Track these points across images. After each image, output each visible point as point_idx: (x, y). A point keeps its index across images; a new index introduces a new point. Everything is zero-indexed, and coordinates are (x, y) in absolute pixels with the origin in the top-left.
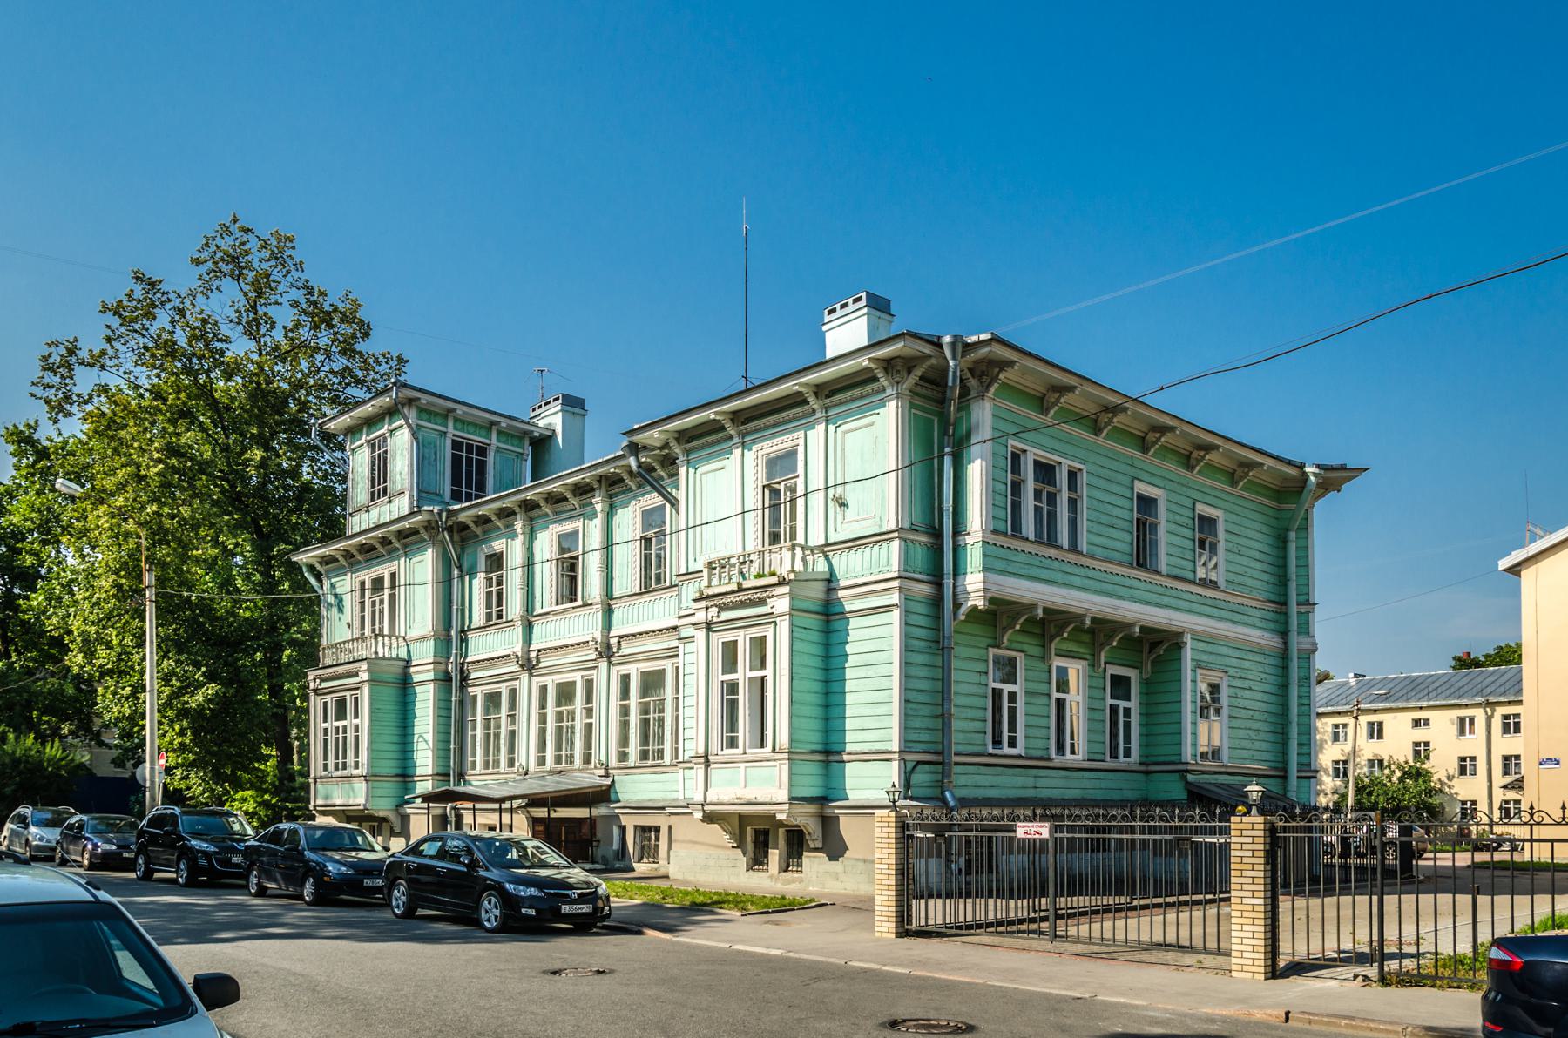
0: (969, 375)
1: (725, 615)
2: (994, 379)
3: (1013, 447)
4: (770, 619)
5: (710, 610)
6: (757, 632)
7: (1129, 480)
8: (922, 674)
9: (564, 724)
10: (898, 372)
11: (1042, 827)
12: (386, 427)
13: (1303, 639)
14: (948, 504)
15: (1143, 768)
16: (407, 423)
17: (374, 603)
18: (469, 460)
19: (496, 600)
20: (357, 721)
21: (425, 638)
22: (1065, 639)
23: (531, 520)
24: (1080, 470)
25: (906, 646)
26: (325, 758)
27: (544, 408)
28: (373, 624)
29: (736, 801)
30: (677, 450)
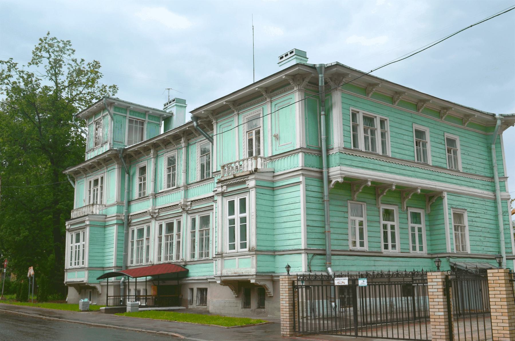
0: (330, 80)
1: (230, 189)
2: (341, 81)
3: (352, 110)
4: (247, 190)
5: (223, 187)
6: (242, 196)
7: (411, 123)
8: (315, 213)
9: (169, 242)
10: (299, 80)
11: (345, 279)
12: (101, 115)
13: (504, 194)
14: (323, 137)
15: (430, 256)
16: (109, 112)
17: (94, 190)
19: (142, 186)
20: (84, 243)
21: (113, 205)
22: (410, 199)
23: (157, 151)
24: (386, 120)
25: (306, 200)
26: (71, 260)
27: (169, 104)
28: (94, 199)
29: (234, 275)
30: (211, 117)
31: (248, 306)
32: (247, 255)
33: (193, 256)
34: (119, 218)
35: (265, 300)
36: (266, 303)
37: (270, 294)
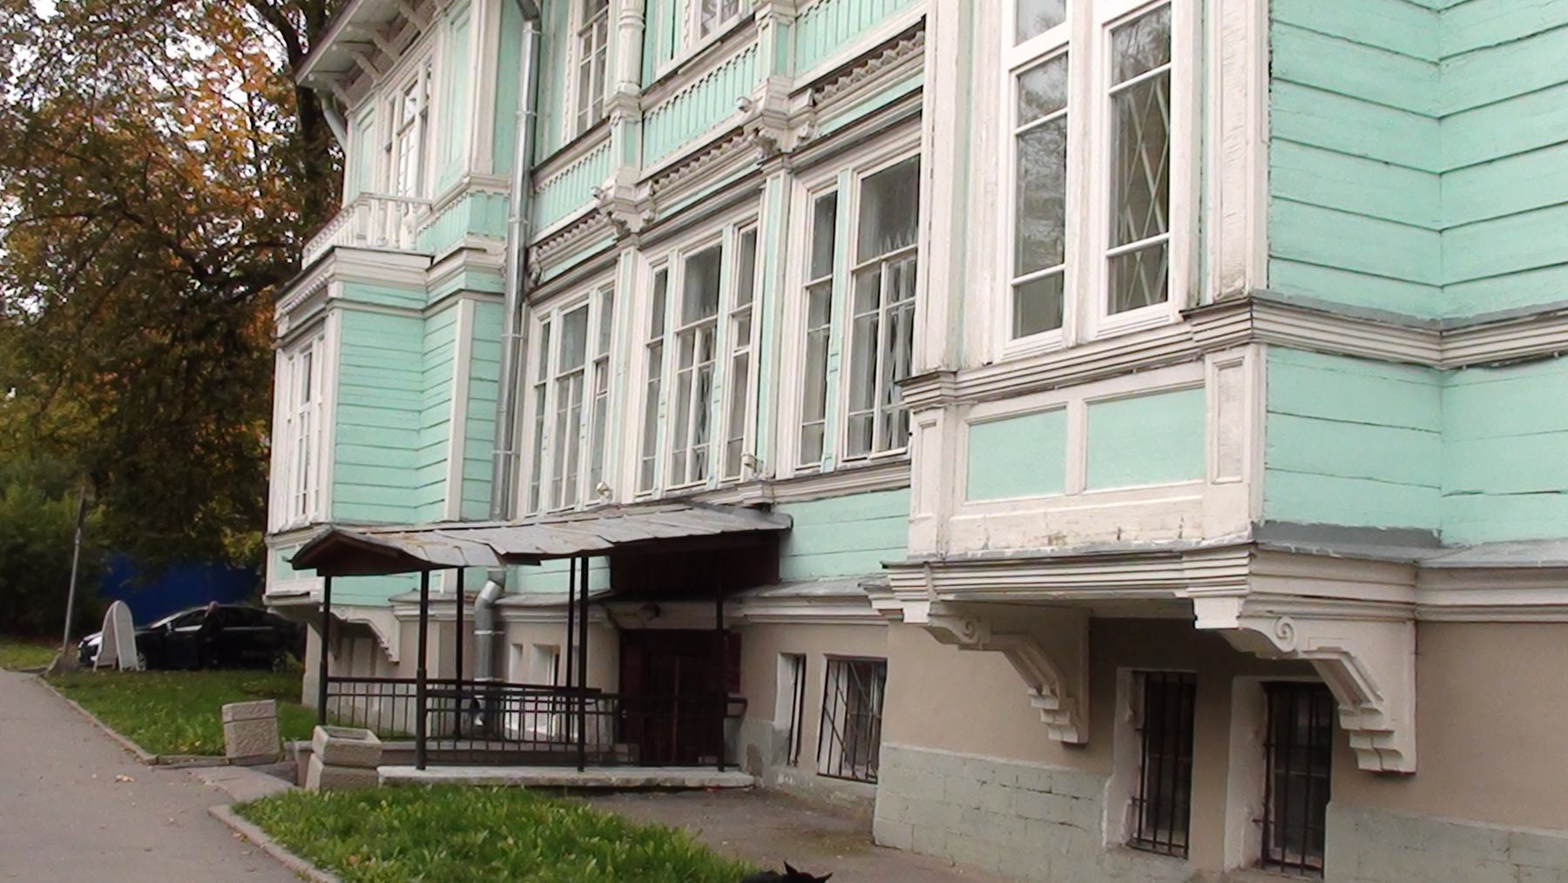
19: (593, 73)
29: (1047, 550)
31: (1163, 837)
32: (1170, 362)
33: (813, 440)
34: (475, 258)
35: (1326, 797)
36: (1336, 820)
37: (1379, 752)
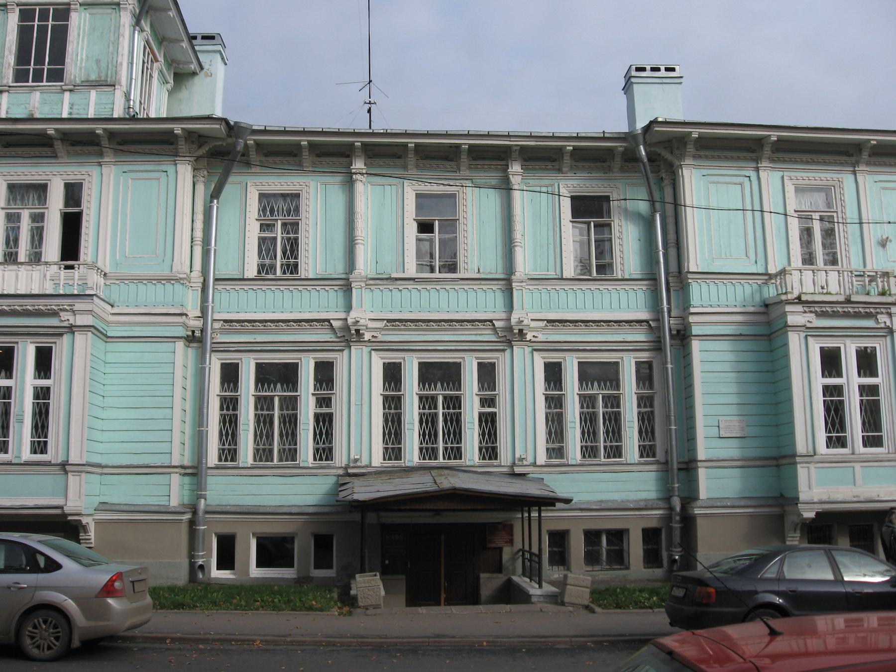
18: (43, 30)
